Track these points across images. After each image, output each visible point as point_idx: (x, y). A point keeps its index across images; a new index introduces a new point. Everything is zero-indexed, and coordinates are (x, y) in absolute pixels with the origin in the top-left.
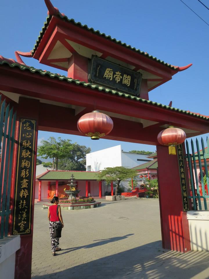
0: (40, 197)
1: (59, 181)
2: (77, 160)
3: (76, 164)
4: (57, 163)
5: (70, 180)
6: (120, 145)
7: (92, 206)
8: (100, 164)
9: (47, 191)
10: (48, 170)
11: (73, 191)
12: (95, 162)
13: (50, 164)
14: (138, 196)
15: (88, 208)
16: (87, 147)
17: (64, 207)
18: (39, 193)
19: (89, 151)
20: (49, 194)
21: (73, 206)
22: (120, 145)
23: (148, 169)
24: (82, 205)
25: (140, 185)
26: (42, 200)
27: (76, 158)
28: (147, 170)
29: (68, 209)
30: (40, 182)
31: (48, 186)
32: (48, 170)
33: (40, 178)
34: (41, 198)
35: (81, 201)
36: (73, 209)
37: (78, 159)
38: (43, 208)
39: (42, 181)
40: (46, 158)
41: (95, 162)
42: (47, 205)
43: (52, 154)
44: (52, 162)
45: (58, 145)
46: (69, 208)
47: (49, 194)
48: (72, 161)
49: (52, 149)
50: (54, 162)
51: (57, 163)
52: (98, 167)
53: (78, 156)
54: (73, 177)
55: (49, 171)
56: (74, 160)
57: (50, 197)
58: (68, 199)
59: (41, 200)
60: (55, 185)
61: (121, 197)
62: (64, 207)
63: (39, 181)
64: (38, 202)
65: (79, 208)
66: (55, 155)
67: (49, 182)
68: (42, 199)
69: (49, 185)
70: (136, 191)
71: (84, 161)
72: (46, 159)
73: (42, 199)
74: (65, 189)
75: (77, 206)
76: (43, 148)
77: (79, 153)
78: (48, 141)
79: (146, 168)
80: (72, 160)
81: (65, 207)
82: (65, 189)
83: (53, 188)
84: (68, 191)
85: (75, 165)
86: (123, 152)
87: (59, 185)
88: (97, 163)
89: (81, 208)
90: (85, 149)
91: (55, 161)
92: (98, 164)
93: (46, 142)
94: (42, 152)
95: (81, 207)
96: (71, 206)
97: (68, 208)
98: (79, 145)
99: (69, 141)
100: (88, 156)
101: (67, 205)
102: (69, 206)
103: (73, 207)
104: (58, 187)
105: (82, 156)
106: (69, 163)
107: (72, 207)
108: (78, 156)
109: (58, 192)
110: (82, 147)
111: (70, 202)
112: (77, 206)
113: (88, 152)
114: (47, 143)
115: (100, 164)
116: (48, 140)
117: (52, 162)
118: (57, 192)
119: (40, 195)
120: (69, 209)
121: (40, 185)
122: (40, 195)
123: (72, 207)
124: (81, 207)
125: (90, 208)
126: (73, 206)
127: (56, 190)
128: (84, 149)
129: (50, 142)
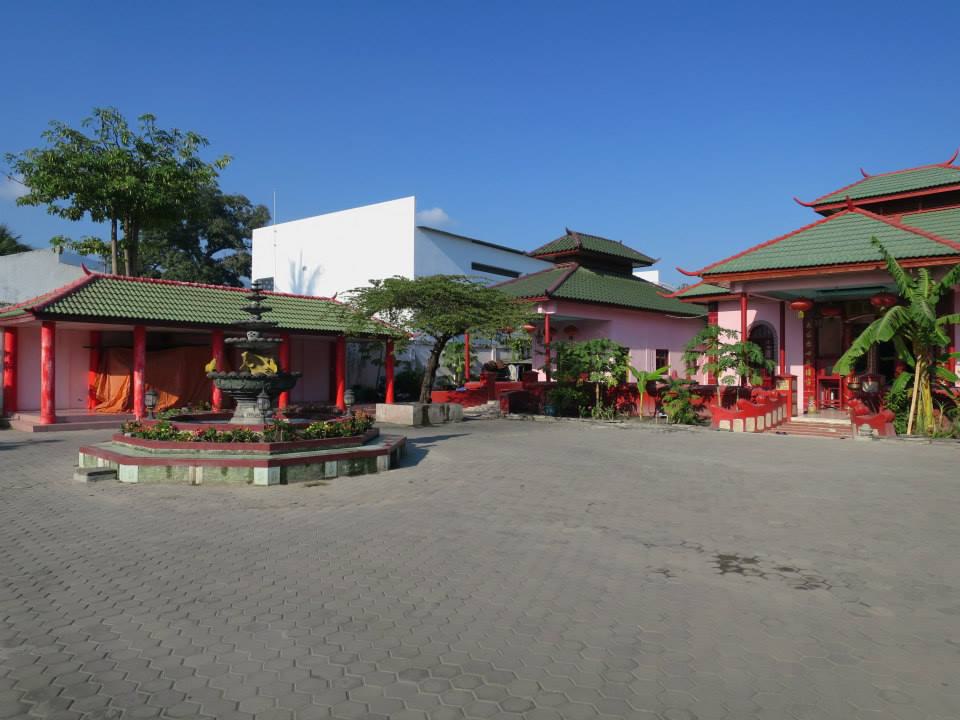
0: (48, 403)
1: (150, 328)
2: (211, 253)
3: (204, 271)
4: (131, 244)
5: (240, 328)
6: (413, 198)
7: (382, 461)
8: (317, 273)
9: (89, 378)
10: (88, 273)
11: (262, 377)
12: (293, 266)
13: (97, 246)
14: (507, 406)
15: (361, 472)
16: (255, 202)
17: (224, 472)
18: (44, 385)
19: (262, 219)
20: (92, 391)
21: (284, 465)
22: (413, 198)
23: (550, 298)
24: (331, 458)
25: (483, 363)
26: (64, 420)
27: (203, 243)
28: (545, 305)
29: (250, 482)
30: (44, 331)
31: (88, 351)
34: (53, 409)
35: (319, 434)
36: (284, 481)
37: (214, 247)
38: (80, 471)
39: (60, 325)
40: (76, 216)
41: (293, 266)
42: (107, 455)
43: (110, 196)
44: (107, 240)
45: (138, 156)
46: (262, 475)
47: (92, 391)
48: (188, 257)
49: (105, 169)
50: (119, 239)
52: (306, 284)
53: (211, 238)
54: (259, 299)
55: (97, 278)
56: (198, 254)
58: (233, 421)
59: (53, 418)
60: (132, 347)
61: (448, 409)
62: (224, 472)
63: (39, 323)
64: (37, 429)
65: (315, 476)
66: (122, 207)
67: (93, 333)
68: (58, 414)
69: (92, 348)
70: (484, 388)
71: (242, 259)
72: (74, 219)
73: (58, 414)
74: (210, 367)
75: (306, 462)
76: (62, 161)
77: (217, 225)
78: (89, 133)
79: (547, 293)
80: (186, 249)
81: (230, 468)
82: (213, 362)
84: (235, 378)
85: (200, 272)
86: (422, 229)
87: (148, 349)
88: (304, 268)
89: (328, 474)
90: (244, 210)
91: (121, 235)
92: (307, 275)
93: (73, 133)
94: (56, 181)
95: (328, 464)
96: (271, 464)
97: (251, 475)
98: (219, 192)
99: (196, 140)
100: (261, 238)
101: (240, 455)
102: (260, 464)
103: (284, 472)
105: (231, 238)
106: (173, 265)
107: (277, 470)
108: (217, 235)
109: (146, 379)
110: (230, 201)
111: (255, 440)
112: (306, 462)
113: (261, 224)
114: (80, 140)
115: (317, 273)
116: (85, 124)
117: (107, 240)
118: (138, 382)
119: (52, 395)
120: (256, 481)
121: (45, 343)
122: (52, 395)
123: (277, 470)
124: (328, 464)
125: (373, 470)
126: (284, 465)
127: (136, 373)
128: (240, 209)
129: (98, 138)
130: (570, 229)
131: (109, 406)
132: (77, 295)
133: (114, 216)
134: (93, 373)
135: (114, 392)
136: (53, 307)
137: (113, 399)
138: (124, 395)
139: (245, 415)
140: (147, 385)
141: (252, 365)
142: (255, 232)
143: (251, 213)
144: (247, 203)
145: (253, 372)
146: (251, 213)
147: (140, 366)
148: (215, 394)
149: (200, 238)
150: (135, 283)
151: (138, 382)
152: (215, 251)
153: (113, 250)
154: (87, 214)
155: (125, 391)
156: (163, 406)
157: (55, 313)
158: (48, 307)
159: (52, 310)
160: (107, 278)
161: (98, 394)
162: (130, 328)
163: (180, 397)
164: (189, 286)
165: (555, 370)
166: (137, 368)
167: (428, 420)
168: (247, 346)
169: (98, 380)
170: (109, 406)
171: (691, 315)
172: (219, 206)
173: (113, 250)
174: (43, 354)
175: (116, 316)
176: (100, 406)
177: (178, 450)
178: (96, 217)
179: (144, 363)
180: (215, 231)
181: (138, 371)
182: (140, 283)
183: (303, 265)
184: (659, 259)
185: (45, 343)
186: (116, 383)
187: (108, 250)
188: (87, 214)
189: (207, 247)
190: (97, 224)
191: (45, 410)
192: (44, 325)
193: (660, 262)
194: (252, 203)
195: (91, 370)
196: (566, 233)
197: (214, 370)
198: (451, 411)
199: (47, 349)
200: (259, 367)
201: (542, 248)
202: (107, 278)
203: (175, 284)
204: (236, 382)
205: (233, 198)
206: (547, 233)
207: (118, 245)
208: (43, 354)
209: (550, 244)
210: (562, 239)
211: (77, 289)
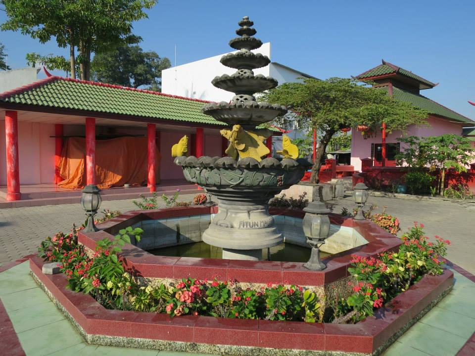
0: (13, 182)
1: (99, 121)
6: (269, 43)
9: (54, 160)
10: (49, 75)
11: (254, 168)
16: (162, 56)
18: (9, 167)
19: (167, 64)
20: (57, 171)
22: (269, 43)
24: (366, 335)
26: (27, 196)
30: (8, 119)
31: (53, 141)
32: (49, 75)
33: (9, 95)
39: (22, 115)
40: (44, 38)
47: (57, 171)
51: (85, 62)
55: (55, 79)
57: (62, 179)
59: (17, 195)
60: (85, 137)
68: (23, 190)
69: (56, 137)
83: (72, 149)
84: (231, 167)
90: (155, 61)
98: (141, 49)
104: (96, 143)
108: (140, 75)
109: (95, 162)
110: (147, 55)
117: (69, 58)
118: (90, 165)
119: (16, 175)
121: (8, 130)
122: (16, 175)
127: (88, 157)
130: (385, 61)
131: (68, 183)
132: (38, 90)
133: (74, 43)
134: (57, 156)
135: (72, 172)
136: (14, 98)
137: (71, 177)
138: (79, 175)
139: (236, 225)
140: (97, 167)
141: (242, 147)
142: (164, 72)
143: (160, 62)
144: (157, 57)
145: (242, 156)
146: (160, 62)
147: (91, 151)
148: (149, 174)
149: (130, 78)
150: (87, 85)
151: (90, 165)
152: (139, 85)
153: (72, 65)
154: (53, 38)
155: (80, 171)
156: (110, 183)
157: (14, 103)
158: (9, 98)
159: (18, 101)
160: (64, 80)
161: (61, 173)
162: (81, 120)
163: (123, 176)
164: (128, 90)
165: (417, 154)
166: (88, 152)
167: (322, 199)
168: (239, 115)
169: (61, 162)
170: (68, 183)
171: (455, 120)
172: (141, 58)
173: (72, 65)
174: (7, 139)
175: (74, 108)
176: (62, 183)
177: (148, 341)
178: (61, 43)
179: (94, 149)
180: (139, 72)
181: (90, 156)
182: (91, 85)
183: (193, 91)
184: (437, 84)
185: (8, 130)
186: (74, 164)
187: (69, 64)
188: (53, 38)
189: (134, 83)
190: (62, 48)
191: (11, 188)
192: (8, 113)
193: (438, 85)
194: (160, 57)
195: (56, 154)
196: (382, 63)
197: (184, 154)
198: (337, 190)
199: (10, 135)
200: (251, 149)
201: (364, 74)
202: (64, 80)
203: (118, 88)
204: (230, 173)
205: (149, 53)
206: (370, 63)
207: (75, 62)
208: (7, 139)
209: (370, 71)
210: (378, 68)
211: (37, 86)
